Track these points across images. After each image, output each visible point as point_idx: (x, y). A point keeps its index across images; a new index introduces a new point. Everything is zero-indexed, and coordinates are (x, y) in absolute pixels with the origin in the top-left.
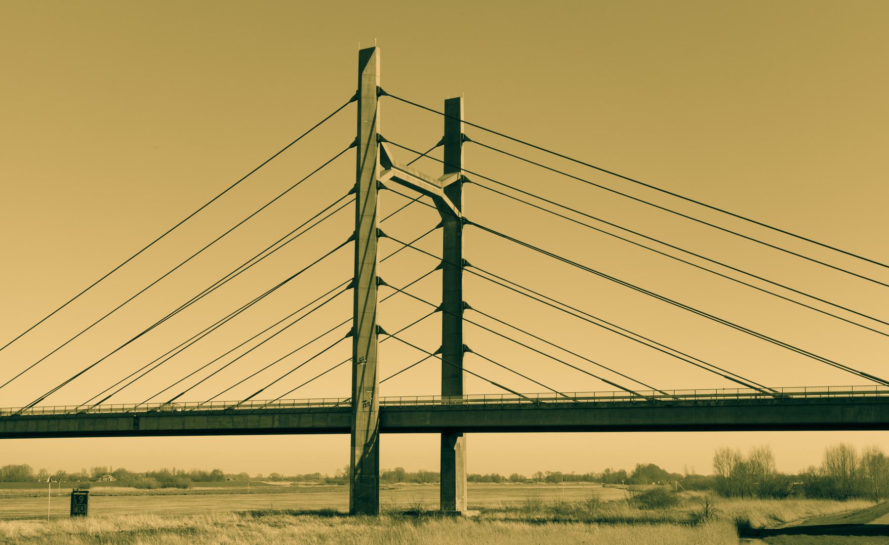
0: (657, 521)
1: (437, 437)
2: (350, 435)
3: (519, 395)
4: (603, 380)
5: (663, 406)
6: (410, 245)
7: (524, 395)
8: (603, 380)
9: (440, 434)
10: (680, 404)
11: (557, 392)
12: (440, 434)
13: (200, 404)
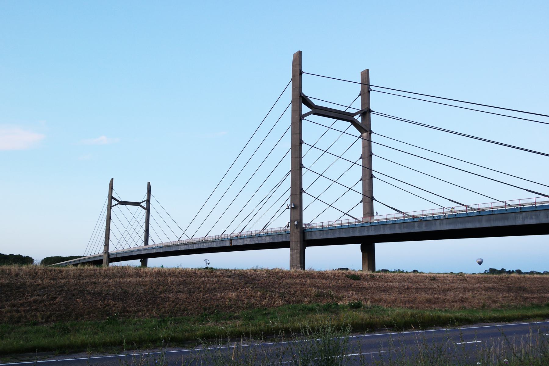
0: (532, 318)
1: (357, 247)
2: (289, 248)
3: (467, 206)
4: (527, 190)
5: (418, 220)
6: (141, 204)
7: (470, 206)
8: (527, 190)
9: (375, 243)
10: (426, 219)
11: (444, 208)
12: (375, 243)
13: (245, 233)
